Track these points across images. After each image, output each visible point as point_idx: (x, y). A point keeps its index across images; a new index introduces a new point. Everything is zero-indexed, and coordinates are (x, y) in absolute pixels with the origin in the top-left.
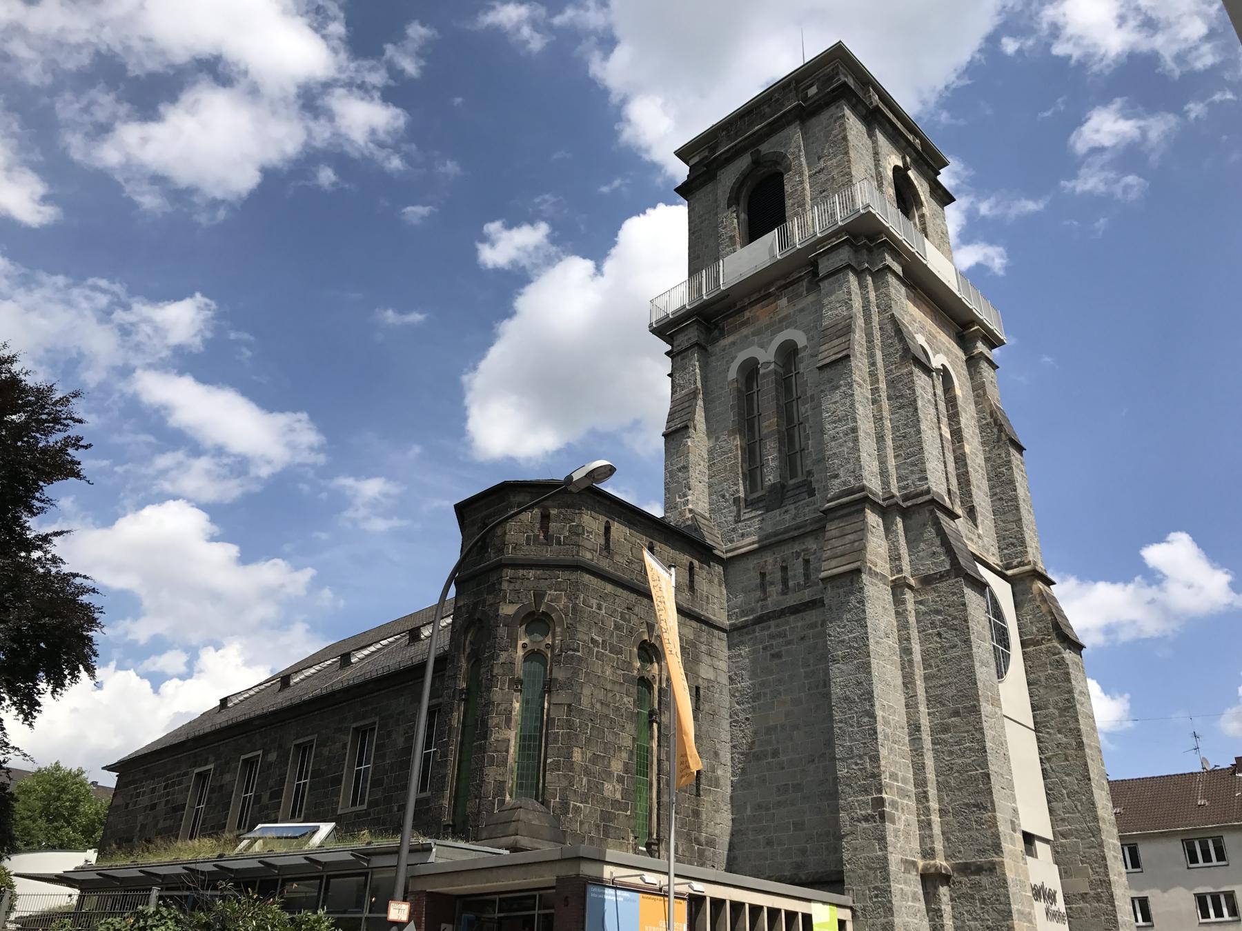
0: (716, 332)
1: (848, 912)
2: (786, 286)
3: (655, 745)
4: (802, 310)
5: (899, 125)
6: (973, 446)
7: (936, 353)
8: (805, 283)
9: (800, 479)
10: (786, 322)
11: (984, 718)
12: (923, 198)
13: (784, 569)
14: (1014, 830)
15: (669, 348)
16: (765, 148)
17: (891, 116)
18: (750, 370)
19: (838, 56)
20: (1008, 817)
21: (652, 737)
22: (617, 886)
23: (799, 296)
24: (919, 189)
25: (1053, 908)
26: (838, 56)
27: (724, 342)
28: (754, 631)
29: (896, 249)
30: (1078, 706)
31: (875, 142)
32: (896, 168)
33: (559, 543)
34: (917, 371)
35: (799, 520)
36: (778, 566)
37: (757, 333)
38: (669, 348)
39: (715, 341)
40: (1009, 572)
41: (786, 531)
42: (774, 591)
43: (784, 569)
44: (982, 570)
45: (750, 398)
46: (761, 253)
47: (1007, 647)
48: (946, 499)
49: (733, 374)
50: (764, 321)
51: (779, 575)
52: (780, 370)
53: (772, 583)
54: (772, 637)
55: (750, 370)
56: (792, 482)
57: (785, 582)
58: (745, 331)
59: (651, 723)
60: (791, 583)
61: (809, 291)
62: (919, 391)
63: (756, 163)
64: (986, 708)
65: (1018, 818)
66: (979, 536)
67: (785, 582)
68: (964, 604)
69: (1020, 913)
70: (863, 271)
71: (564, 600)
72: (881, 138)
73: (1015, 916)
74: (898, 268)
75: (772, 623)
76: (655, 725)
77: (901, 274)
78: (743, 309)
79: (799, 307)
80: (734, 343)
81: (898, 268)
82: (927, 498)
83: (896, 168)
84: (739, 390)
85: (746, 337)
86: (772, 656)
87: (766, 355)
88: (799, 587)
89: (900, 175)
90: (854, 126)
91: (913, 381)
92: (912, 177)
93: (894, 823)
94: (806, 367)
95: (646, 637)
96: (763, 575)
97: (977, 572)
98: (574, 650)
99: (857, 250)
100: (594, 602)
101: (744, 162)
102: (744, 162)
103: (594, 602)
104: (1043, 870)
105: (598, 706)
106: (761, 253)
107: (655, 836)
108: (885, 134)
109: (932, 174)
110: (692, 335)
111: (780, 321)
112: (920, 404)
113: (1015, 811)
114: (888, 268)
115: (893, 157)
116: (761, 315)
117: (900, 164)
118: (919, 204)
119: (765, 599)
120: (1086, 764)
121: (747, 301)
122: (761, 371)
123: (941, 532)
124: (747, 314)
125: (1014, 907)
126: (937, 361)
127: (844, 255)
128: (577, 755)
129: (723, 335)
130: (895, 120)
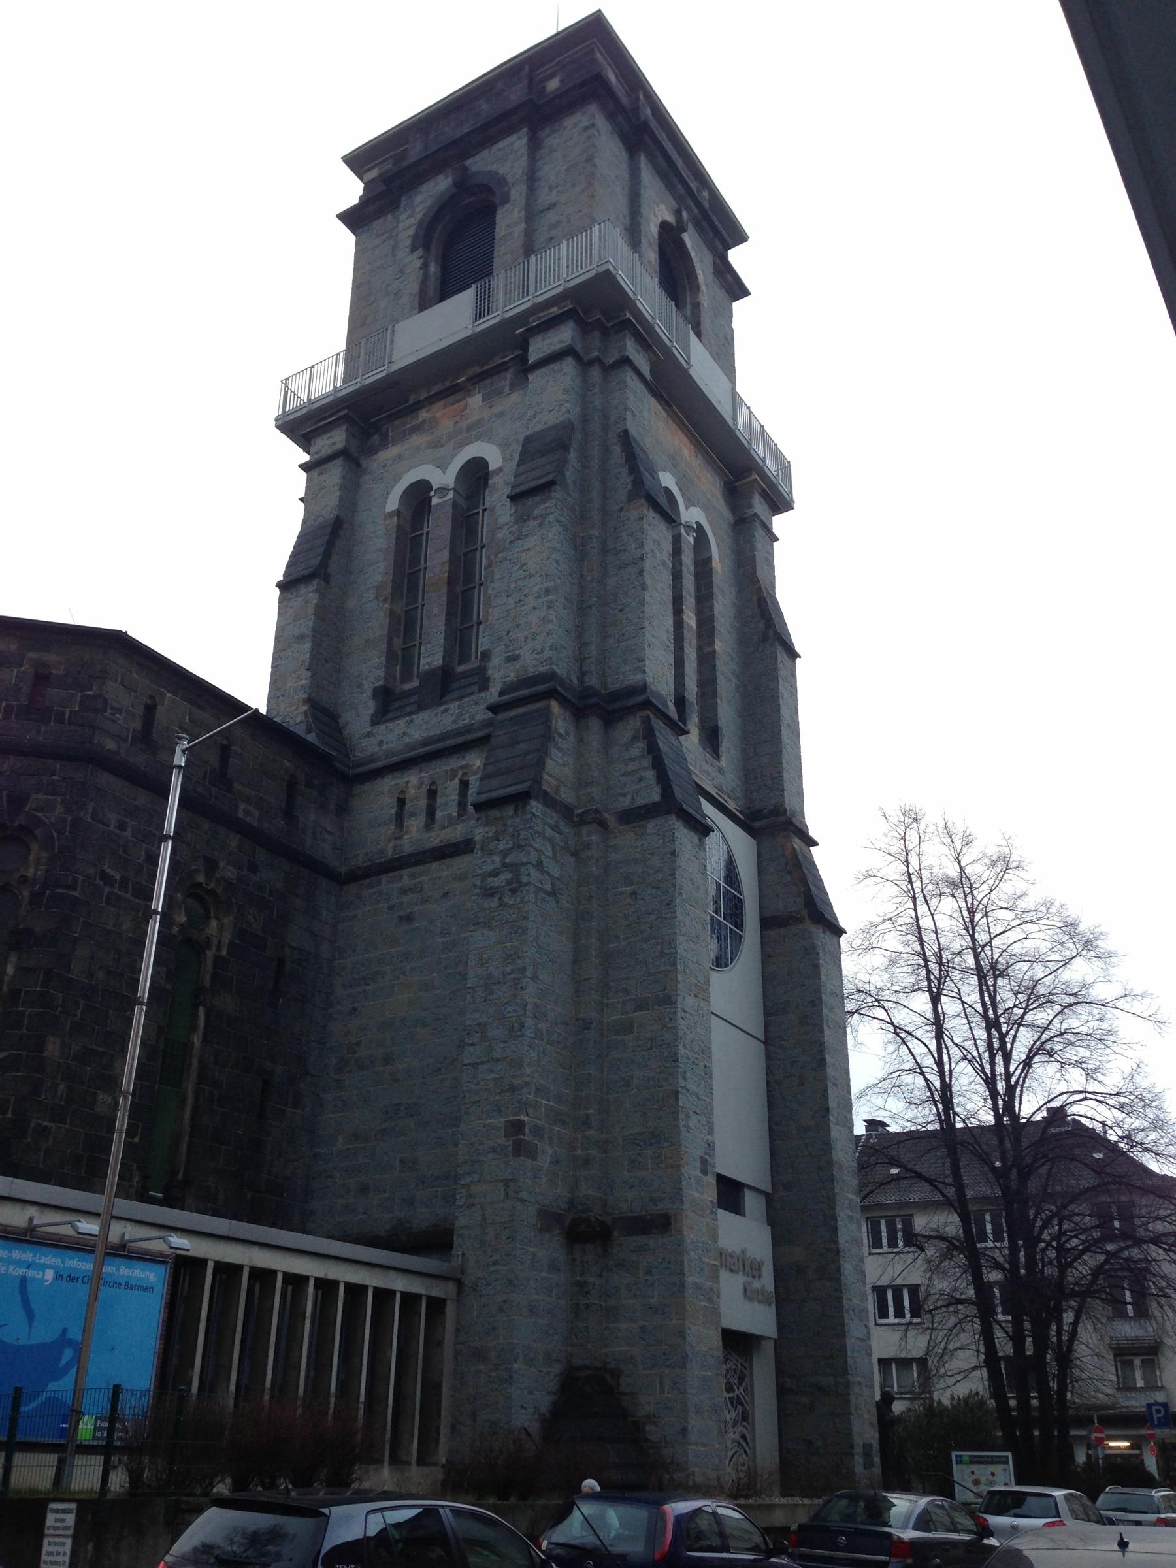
0: (376, 438)
1: (452, 1287)
2: (480, 378)
3: (197, 1040)
4: (501, 415)
5: (680, 163)
6: (724, 645)
7: (689, 503)
8: (509, 375)
9: (473, 664)
10: (477, 431)
11: (680, 1013)
12: (701, 277)
13: (432, 794)
14: (705, 1172)
15: (306, 458)
16: (482, 163)
17: (668, 146)
18: (419, 494)
19: (594, 33)
20: (698, 1153)
21: (193, 1028)
23: (499, 392)
24: (697, 266)
25: (757, 1284)
26: (594, 33)
27: (384, 455)
28: (379, 883)
29: (647, 339)
30: (825, 1011)
32: (664, 225)
33: (60, 719)
34: (651, 515)
35: (461, 723)
36: (424, 789)
37: (437, 444)
38: (306, 458)
39: (373, 451)
40: (757, 824)
42: (414, 824)
43: (432, 794)
44: (708, 809)
45: (416, 542)
46: (453, 321)
47: (740, 925)
48: (672, 707)
49: (393, 504)
50: (446, 426)
51: (423, 803)
52: (463, 503)
53: (413, 814)
54: (404, 892)
55: (419, 494)
56: (460, 669)
57: (431, 813)
58: (417, 440)
59: (196, 1006)
60: (439, 815)
61: (513, 387)
62: (649, 546)
63: (463, 186)
64: (686, 1001)
65: (712, 1156)
66: (721, 770)
67: (431, 813)
68: (673, 853)
69: (698, 1287)
70: (591, 363)
71: (59, 810)
72: (643, 161)
73: (689, 1292)
74: (643, 364)
75: (406, 872)
76: (201, 1011)
77: (648, 377)
78: (418, 406)
79: (497, 409)
80: (400, 457)
81: (643, 364)
82: (640, 699)
83: (664, 225)
84: (399, 528)
85: (418, 449)
86: (401, 918)
87: (443, 478)
88: (451, 821)
89: (670, 237)
90: (610, 151)
91: (642, 530)
92: (689, 244)
93: (534, 1158)
94: (497, 498)
95: (201, 878)
96: (401, 802)
97: (699, 809)
98: (68, 887)
99: (585, 328)
100: (113, 818)
101: (441, 184)
102: (441, 184)
103: (113, 818)
104: (746, 1234)
105: (101, 975)
106: (453, 321)
107: (180, 1176)
108: (652, 160)
109: (720, 247)
110: (337, 438)
111: (469, 429)
112: (648, 564)
113: (710, 1146)
114: (626, 361)
115: (663, 207)
116: (442, 418)
117: (670, 218)
118: (695, 288)
119: (399, 838)
120: (826, 1091)
121: (424, 395)
122: (435, 501)
123: (653, 750)
124: (424, 415)
125: (690, 1279)
126: (690, 515)
127: (564, 335)
128: (53, 1048)
129: (384, 444)
130: (674, 155)
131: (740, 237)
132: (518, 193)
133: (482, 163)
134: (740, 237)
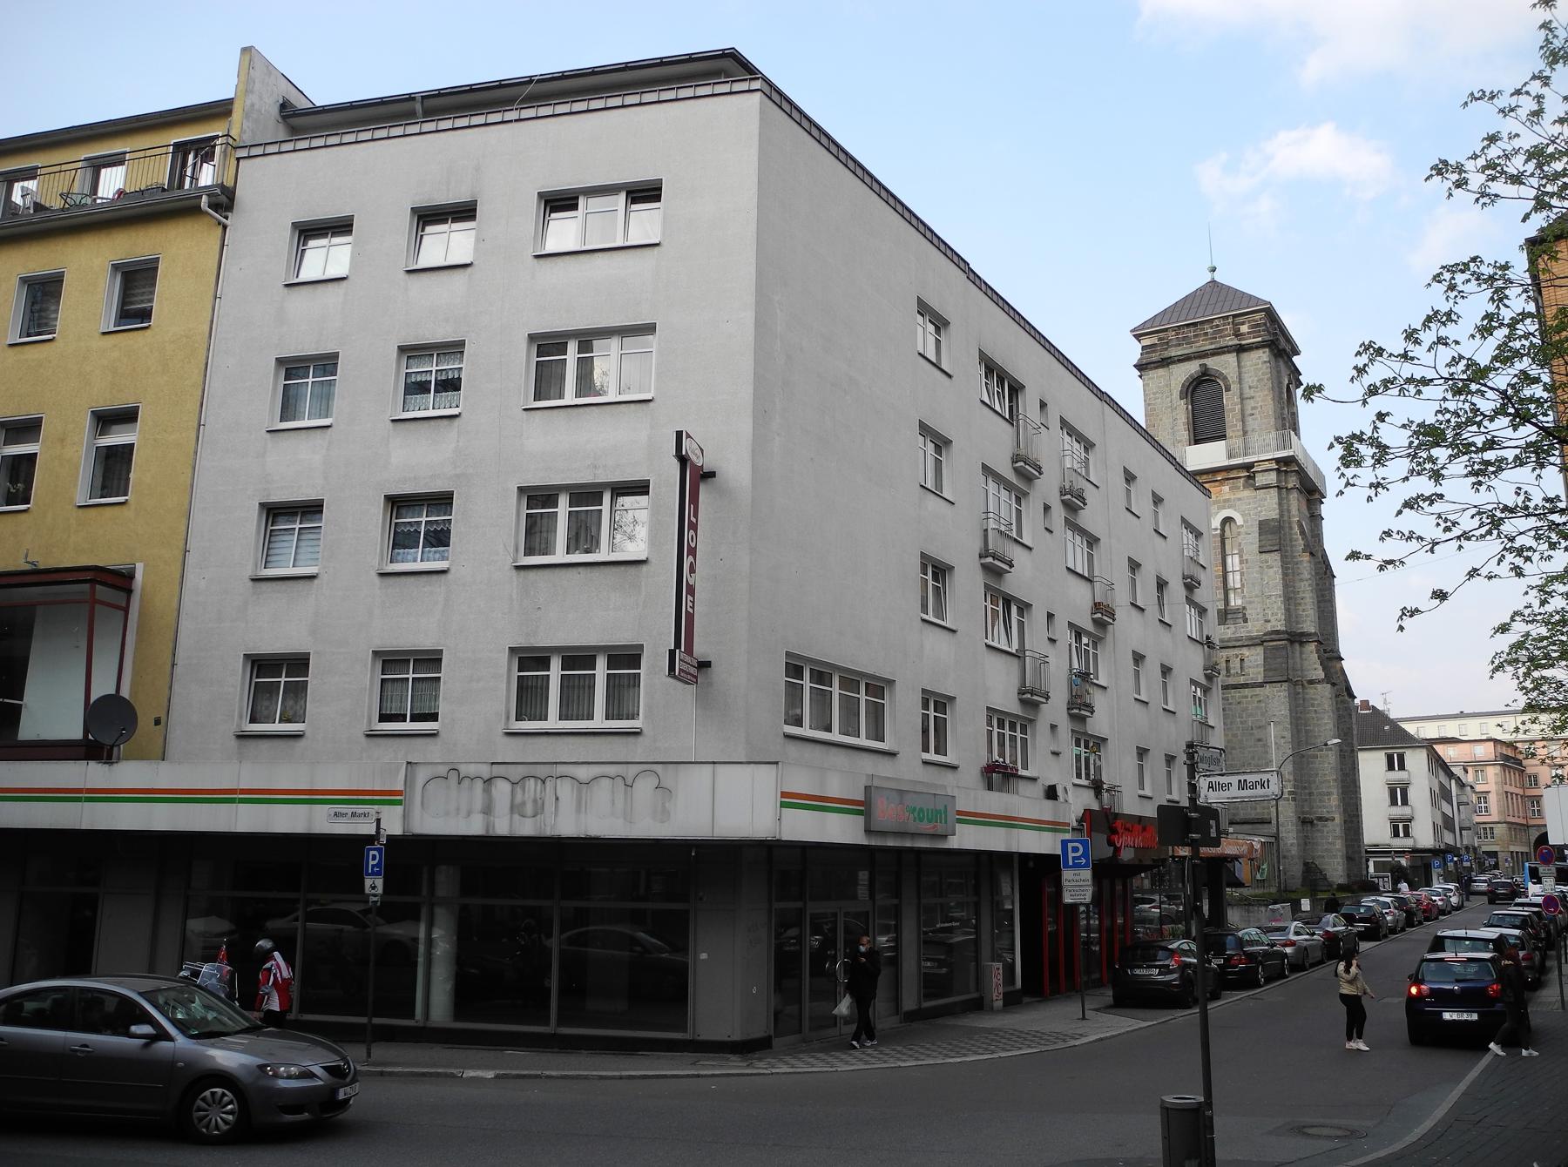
10: (1227, 503)
16: (1212, 363)
22: (102, 603)
31: (1279, 372)
41: (1229, 640)
102: (1193, 368)
131: (1297, 353)
132: (1235, 387)
133: (1212, 363)
134: (1297, 353)
